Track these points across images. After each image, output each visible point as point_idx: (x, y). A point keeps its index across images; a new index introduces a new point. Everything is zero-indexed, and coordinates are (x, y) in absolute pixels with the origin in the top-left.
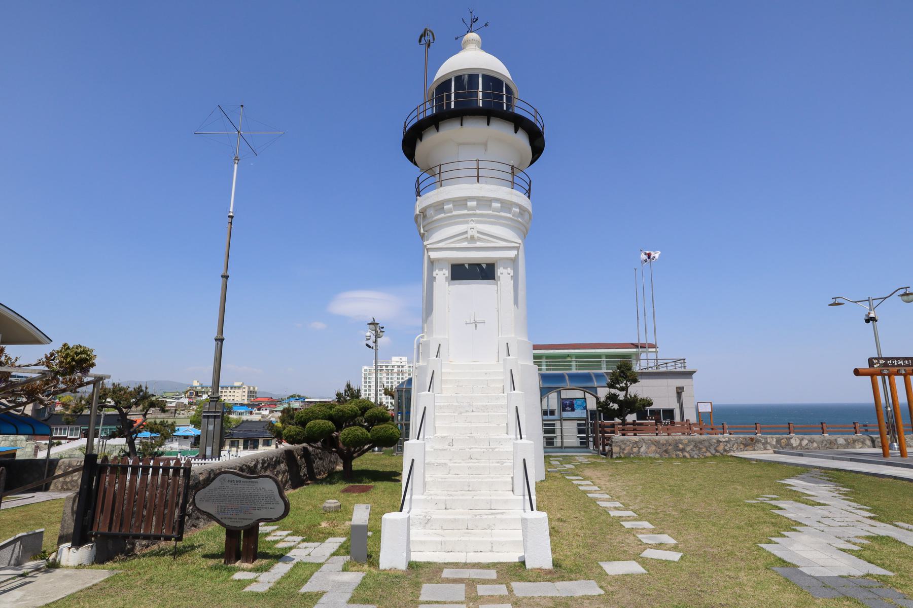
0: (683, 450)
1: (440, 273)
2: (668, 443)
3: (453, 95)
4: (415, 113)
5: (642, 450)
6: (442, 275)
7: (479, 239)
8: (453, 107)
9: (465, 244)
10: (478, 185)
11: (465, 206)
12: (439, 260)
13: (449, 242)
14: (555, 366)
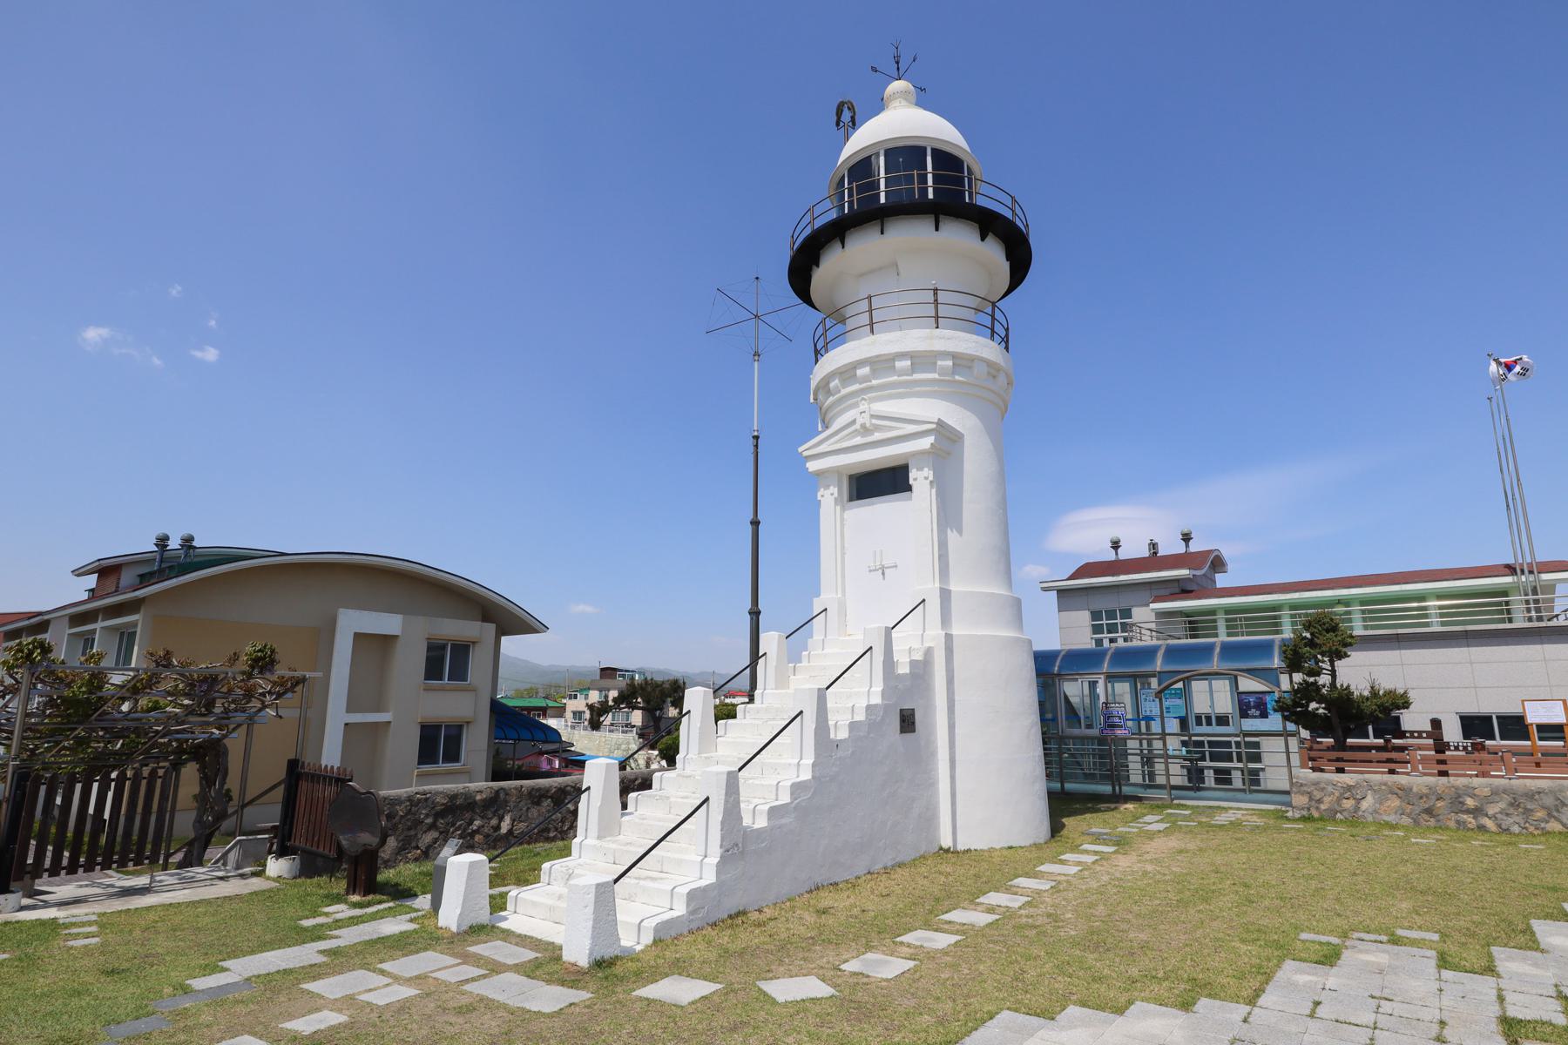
0: (1477, 812)
1: (827, 493)
2: (1433, 793)
3: (930, 177)
4: (808, 218)
5: (1365, 805)
6: (829, 497)
7: (877, 428)
8: (931, 196)
9: (858, 440)
10: (872, 337)
11: (932, 367)
12: (820, 474)
14: (1253, 626)
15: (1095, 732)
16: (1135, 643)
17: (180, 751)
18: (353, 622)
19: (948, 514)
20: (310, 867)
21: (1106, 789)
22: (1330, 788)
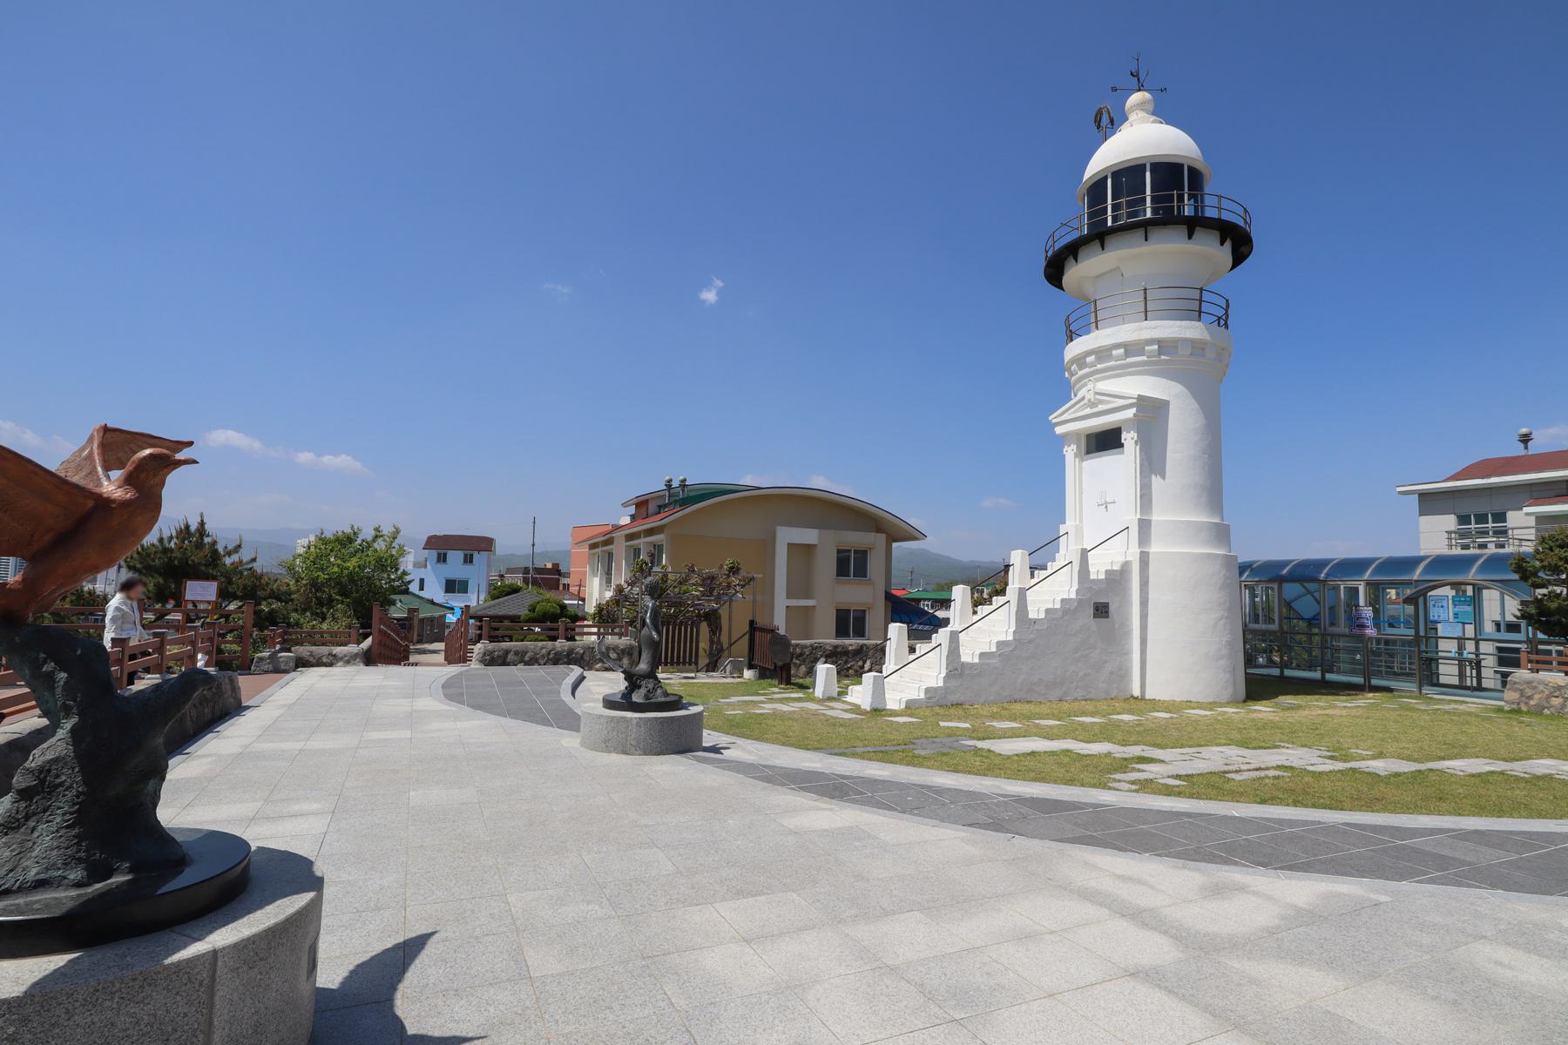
6: (1070, 452)
7: (1101, 402)
9: (1088, 411)
13: (1111, 392)
15: (1274, 627)
16: (1507, 550)
17: (699, 615)
18: (787, 536)
19: (1152, 463)
20: (764, 674)
21: (1359, 680)
22: (1541, 687)
